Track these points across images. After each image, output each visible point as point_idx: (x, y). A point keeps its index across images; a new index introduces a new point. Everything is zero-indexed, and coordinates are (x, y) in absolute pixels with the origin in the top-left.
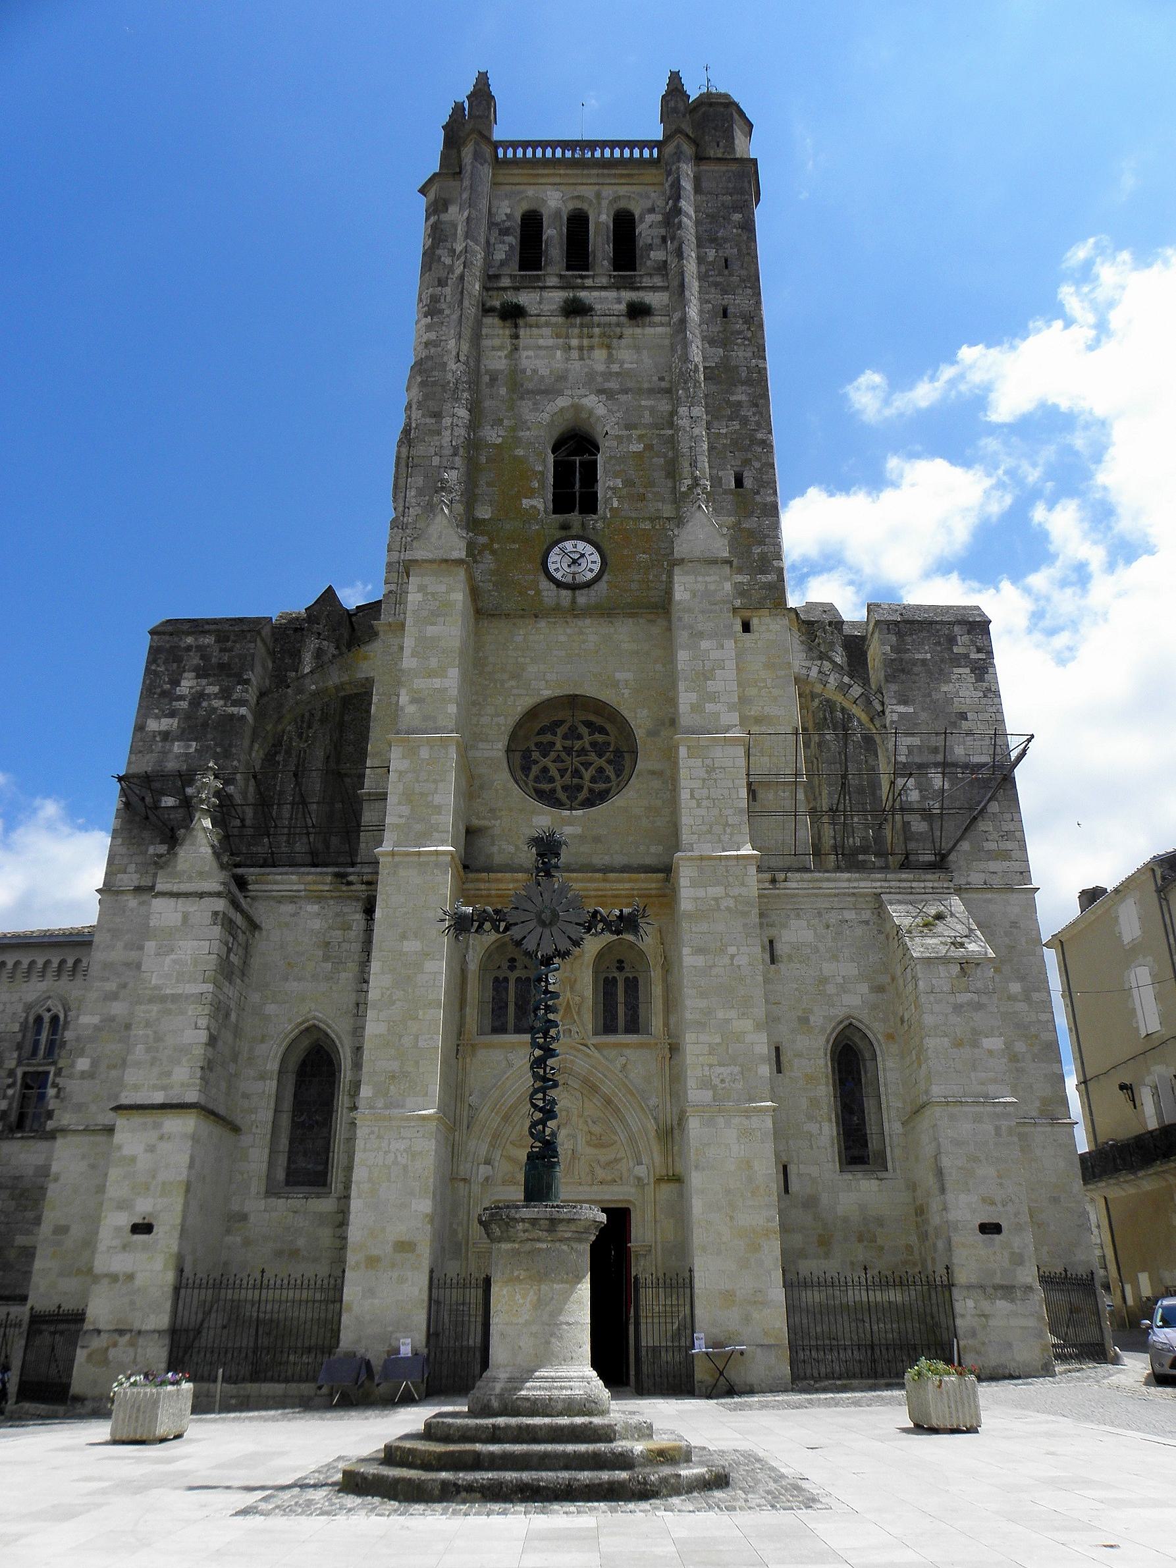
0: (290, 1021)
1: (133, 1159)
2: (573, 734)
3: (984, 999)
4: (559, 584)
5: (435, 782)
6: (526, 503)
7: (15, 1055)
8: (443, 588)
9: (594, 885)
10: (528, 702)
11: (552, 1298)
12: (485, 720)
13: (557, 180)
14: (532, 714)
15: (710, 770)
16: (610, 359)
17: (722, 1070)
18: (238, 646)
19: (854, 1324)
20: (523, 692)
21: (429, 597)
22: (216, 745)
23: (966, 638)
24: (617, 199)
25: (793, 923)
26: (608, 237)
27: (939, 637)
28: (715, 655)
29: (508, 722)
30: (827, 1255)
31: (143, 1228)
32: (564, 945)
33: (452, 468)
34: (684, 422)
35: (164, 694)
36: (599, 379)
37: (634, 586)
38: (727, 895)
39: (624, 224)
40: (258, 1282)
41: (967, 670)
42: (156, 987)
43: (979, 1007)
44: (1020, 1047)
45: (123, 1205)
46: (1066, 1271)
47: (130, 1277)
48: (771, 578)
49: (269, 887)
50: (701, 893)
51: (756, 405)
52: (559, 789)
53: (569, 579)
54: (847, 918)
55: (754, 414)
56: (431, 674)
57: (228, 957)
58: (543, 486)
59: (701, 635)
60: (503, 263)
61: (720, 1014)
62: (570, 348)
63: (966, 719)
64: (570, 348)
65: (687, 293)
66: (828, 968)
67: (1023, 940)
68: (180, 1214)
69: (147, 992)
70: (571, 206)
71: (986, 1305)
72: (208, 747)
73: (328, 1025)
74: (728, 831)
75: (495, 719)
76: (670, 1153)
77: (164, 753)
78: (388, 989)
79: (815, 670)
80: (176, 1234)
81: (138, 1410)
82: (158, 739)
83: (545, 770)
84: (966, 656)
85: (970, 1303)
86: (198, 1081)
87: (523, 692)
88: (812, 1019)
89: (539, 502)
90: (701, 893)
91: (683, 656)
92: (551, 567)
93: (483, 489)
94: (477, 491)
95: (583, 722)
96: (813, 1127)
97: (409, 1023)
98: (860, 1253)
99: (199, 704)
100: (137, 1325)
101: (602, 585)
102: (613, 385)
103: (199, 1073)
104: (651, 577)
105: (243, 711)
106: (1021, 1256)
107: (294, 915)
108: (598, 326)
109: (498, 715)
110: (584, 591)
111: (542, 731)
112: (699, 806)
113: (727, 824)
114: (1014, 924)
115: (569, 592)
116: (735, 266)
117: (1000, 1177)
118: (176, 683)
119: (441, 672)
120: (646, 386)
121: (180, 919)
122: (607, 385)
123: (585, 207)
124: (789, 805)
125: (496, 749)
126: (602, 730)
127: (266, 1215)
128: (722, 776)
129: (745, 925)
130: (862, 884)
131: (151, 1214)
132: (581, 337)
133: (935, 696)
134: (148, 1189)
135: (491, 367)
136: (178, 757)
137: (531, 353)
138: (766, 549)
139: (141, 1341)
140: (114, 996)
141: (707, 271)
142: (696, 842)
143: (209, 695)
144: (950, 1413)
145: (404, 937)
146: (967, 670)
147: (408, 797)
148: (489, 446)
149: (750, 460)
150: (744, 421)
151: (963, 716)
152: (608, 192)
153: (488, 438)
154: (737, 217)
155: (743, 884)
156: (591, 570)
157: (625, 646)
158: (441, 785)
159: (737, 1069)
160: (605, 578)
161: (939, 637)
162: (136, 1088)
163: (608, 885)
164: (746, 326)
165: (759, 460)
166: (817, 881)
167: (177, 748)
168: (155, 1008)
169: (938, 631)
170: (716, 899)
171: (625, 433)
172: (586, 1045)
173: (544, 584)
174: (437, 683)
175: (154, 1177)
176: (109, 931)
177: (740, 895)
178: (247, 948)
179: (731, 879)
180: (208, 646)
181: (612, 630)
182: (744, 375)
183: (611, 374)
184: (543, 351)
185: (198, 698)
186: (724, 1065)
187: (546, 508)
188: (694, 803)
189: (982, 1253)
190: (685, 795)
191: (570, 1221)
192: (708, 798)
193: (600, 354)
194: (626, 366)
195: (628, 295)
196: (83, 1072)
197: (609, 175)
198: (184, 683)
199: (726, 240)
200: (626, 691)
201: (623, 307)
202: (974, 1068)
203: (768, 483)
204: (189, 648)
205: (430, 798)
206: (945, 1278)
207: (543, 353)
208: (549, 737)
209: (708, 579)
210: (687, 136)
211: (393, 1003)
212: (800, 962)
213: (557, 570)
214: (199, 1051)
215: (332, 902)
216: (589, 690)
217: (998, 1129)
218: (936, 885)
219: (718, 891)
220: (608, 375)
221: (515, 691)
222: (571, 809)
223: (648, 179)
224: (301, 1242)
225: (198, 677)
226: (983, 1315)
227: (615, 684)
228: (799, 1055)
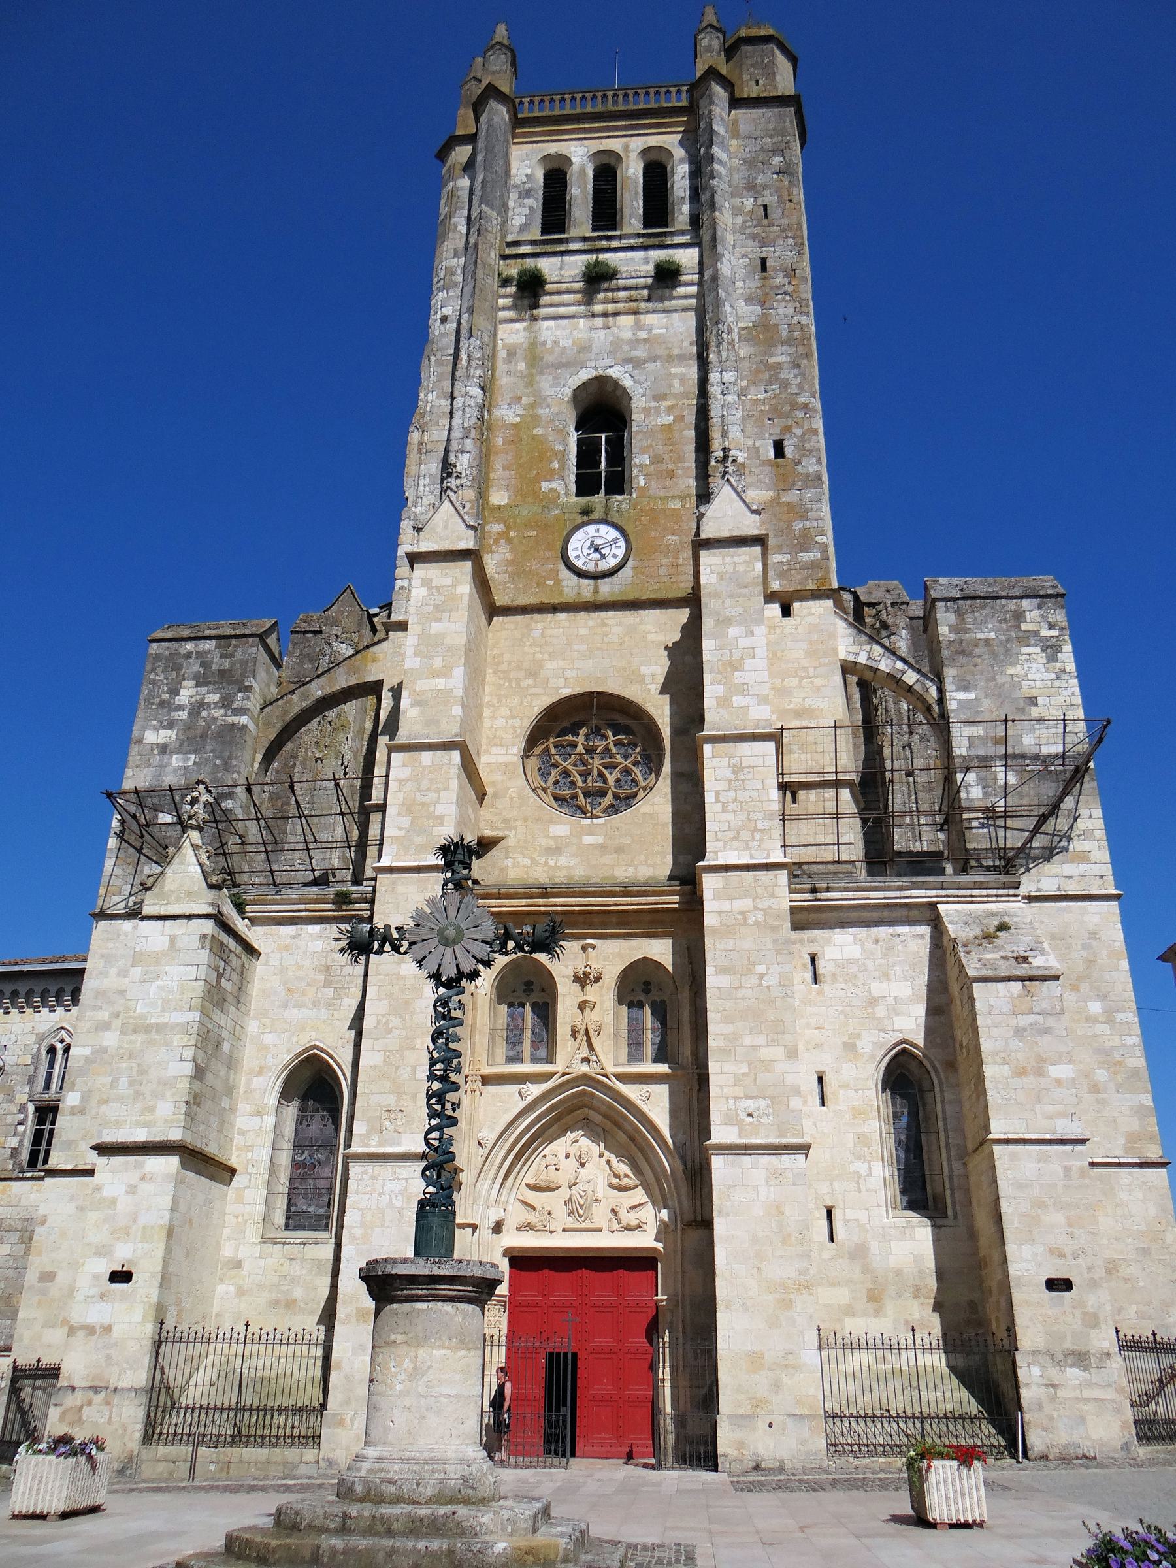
0: (289, 1050)
1: (113, 1202)
3: (1051, 1021)
4: (580, 574)
5: (438, 791)
6: (545, 486)
7: (27, 1089)
8: (448, 581)
10: (547, 701)
11: (430, 1367)
15: (738, 769)
17: (749, 1103)
18: (239, 650)
19: (907, 1393)
20: (540, 690)
21: (434, 591)
22: (215, 757)
23: (1036, 614)
24: (645, 152)
27: (1005, 613)
28: (744, 642)
30: (878, 1313)
31: (121, 1276)
32: (467, 966)
33: (462, 452)
35: (162, 704)
36: (626, 348)
37: (663, 571)
38: (756, 908)
40: (242, 1336)
41: (1038, 649)
42: (142, 1016)
43: (1046, 1031)
44: (1101, 1075)
45: (101, 1251)
46: (1154, 1334)
47: (108, 1329)
50: (726, 906)
51: (799, 366)
55: (796, 376)
56: (434, 674)
57: (218, 982)
59: (728, 622)
61: (747, 1041)
63: (1037, 705)
65: (719, 248)
66: (878, 988)
67: (1104, 952)
68: (160, 1261)
69: (131, 1021)
71: (1054, 1374)
72: (208, 759)
73: (332, 1057)
74: (757, 836)
75: (510, 722)
76: (699, 1197)
77: (162, 766)
78: (384, 1016)
80: (156, 1283)
81: (40, 1482)
82: (156, 752)
84: (1036, 633)
85: (1036, 1371)
86: (183, 1117)
87: (540, 690)
88: (859, 1045)
89: (563, 486)
90: (726, 906)
97: (407, 1052)
99: (199, 713)
100: (113, 1384)
102: (640, 353)
103: (183, 1108)
104: (680, 561)
105: (244, 720)
106: (1095, 1316)
107: (294, 937)
109: (513, 717)
112: (724, 810)
113: (756, 830)
115: (591, 582)
117: (1070, 1225)
118: (174, 692)
119: (445, 672)
120: (676, 352)
121: (167, 944)
122: (634, 353)
124: (830, 807)
127: (262, 1263)
128: (750, 776)
129: (775, 941)
131: (130, 1261)
133: (1000, 679)
134: (128, 1234)
136: (176, 770)
138: (807, 524)
139: (116, 1399)
140: (105, 1026)
141: (744, 222)
143: (208, 704)
144: (948, 1506)
146: (1038, 649)
147: (409, 808)
148: (504, 426)
149: (791, 426)
150: (785, 385)
151: (1033, 701)
152: (638, 143)
153: (505, 418)
154: (777, 160)
155: (773, 895)
156: (615, 556)
157: (652, 637)
158: (444, 794)
160: (630, 563)
161: (1005, 613)
162: (119, 1124)
164: (787, 280)
167: (176, 760)
168: (139, 1038)
169: (1003, 606)
170: (742, 913)
171: (654, 404)
173: (564, 573)
174: (441, 683)
175: (134, 1221)
176: (102, 956)
177: (770, 907)
178: (242, 973)
179: (759, 890)
180: (209, 652)
181: (637, 620)
182: (784, 334)
183: (638, 341)
185: (199, 706)
186: (751, 1098)
187: (567, 490)
188: (719, 807)
189: (1050, 1312)
190: (709, 798)
192: (735, 801)
194: (654, 332)
195: (657, 255)
196: (73, 1108)
198: (183, 692)
201: (650, 268)
202: (1039, 1100)
203: (811, 451)
204: (189, 655)
205: (431, 809)
206: (1005, 1341)
209: (736, 559)
211: (389, 1031)
212: (846, 981)
213: (578, 557)
214: (184, 1085)
217: (1067, 1170)
219: (745, 904)
220: (635, 343)
222: (593, 817)
224: (298, 1293)
225: (197, 685)
226: (1052, 1385)
227: (641, 679)
228: (844, 1086)
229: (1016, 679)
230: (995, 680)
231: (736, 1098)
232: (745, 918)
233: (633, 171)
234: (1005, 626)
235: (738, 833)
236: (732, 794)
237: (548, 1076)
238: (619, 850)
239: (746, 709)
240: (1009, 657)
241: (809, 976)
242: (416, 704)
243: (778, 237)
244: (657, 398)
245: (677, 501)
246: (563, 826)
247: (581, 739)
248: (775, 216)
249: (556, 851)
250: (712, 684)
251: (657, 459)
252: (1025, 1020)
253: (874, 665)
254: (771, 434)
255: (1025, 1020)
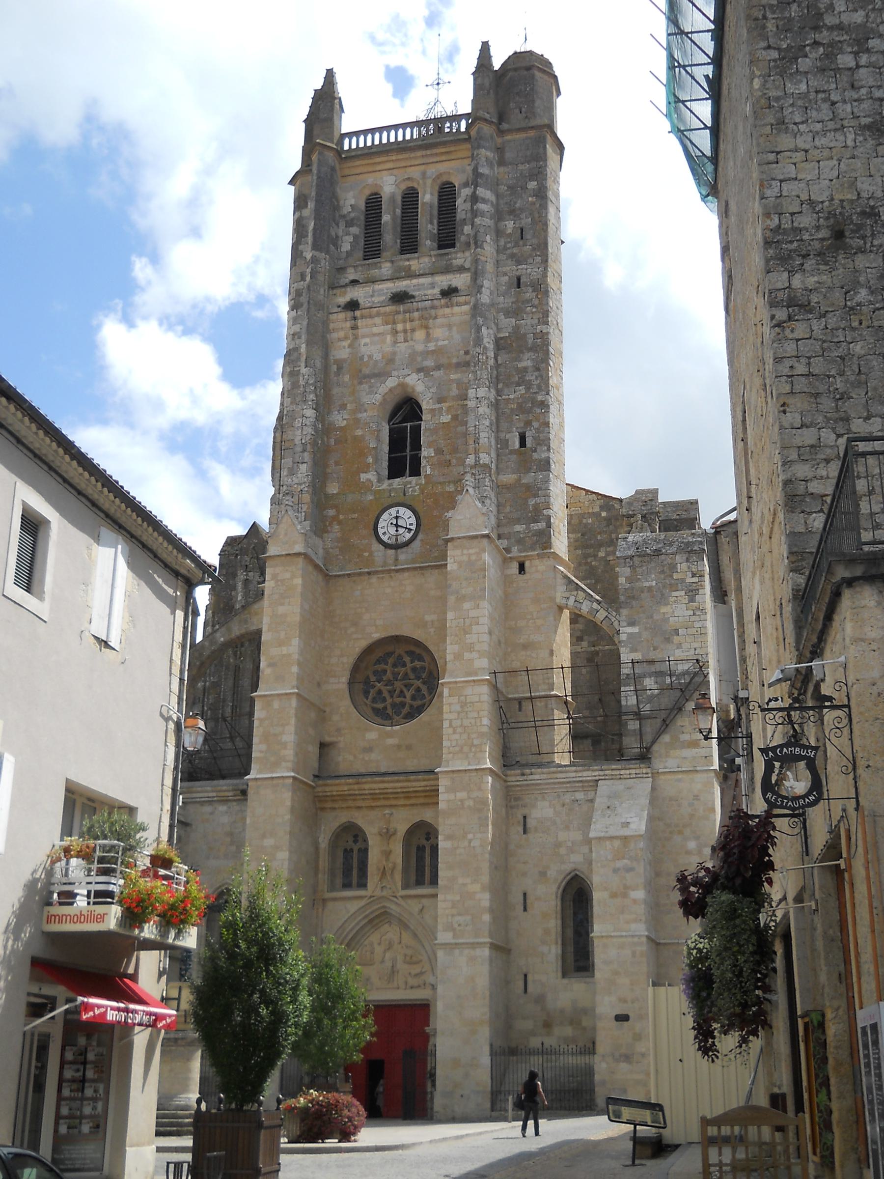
2: (379, 674)
4: (386, 546)
6: (364, 477)
9: (400, 785)
10: (364, 644)
12: (334, 660)
13: (390, 165)
14: (368, 651)
15: (464, 705)
16: (428, 338)
20: (360, 636)
23: (685, 565)
25: (540, 804)
26: (431, 215)
28: (473, 613)
29: (349, 661)
33: (302, 463)
34: (471, 404)
38: (469, 798)
39: (447, 194)
43: (630, 870)
48: (542, 525)
49: (195, 795)
51: (538, 369)
52: (389, 707)
53: (392, 541)
54: (578, 798)
55: (537, 378)
56: (281, 644)
58: (376, 460)
60: (349, 254)
61: (461, 881)
62: (397, 332)
64: (397, 332)
66: (562, 836)
70: (403, 187)
74: (473, 750)
79: (572, 599)
83: (380, 692)
84: (683, 581)
88: (549, 873)
91: (450, 615)
92: (381, 531)
93: (332, 468)
94: (329, 470)
95: (406, 652)
96: (545, 949)
98: (568, 1031)
101: (417, 544)
102: (429, 363)
107: (211, 814)
108: (418, 310)
110: (405, 549)
111: (378, 662)
112: (454, 732)
113: (473, 745)
114: (696, 797)
115: (393, 551)
116: (528, 235)
120: (454, 361)
123: (415, 185)
125: (340, 682)
126: (420, 658)
128: (470, 709)
129: (479, 818)
130: (585, 774)
132: (404, 322)
133: (656, 617)
135: (338, 357)
137: (367, 340)
142: (452, 763)
145: (264, 836)
152: (432, 171)
153: (336, 422)
154: (532, 185)
155: (480, 789)
157: (432, 593)
159: (468, 918)
161: (663, 566)
163: (409, 784)
164: (534, 294)
165: (538, 420)
166: (553, 773)
170: (462, 801)
171: (437, 406)
172: (396, 897)
174: (285, 650)
184: (374, 340)
188: (451, 731)
191: (182, 1039)
193: (420, 335)
197: (432, 155)
199: (522, 210)
200: (432, 630)
201: (437, 291)
203: (543, 441)
207: (376, 338)
208: (383, 666)
209: (471, 551)
210: (486, 120)
213: (384, 533)
215: (234, 803)
216: (407, 631)
218: (638, 771)
220: (426, 354)
221: (355, 636)
223: (460, 155)
229: (666, 616)
230: (652, 617)
231: (453, 916)
232: (462, 804)
233: (428, 197)
234: (662, 576)
235: (462, 748)
236: (459, 722)
237: (361, 897)
238: (409, 747)
239: (471, 660)
240: (663, 599)
241: (521, 829)
242: (270, 665)
243: (530, 256)
244: (440, 400)
245: (452, 485)
246: (373, 733)
247: (388, 668)
248: (529, 237)
249: (369, 750)
250: (451, 644)
251: (439, 451)
252: (619, 864)
253: (579, 606)
254: (517, 428)
255: (619, 864)
